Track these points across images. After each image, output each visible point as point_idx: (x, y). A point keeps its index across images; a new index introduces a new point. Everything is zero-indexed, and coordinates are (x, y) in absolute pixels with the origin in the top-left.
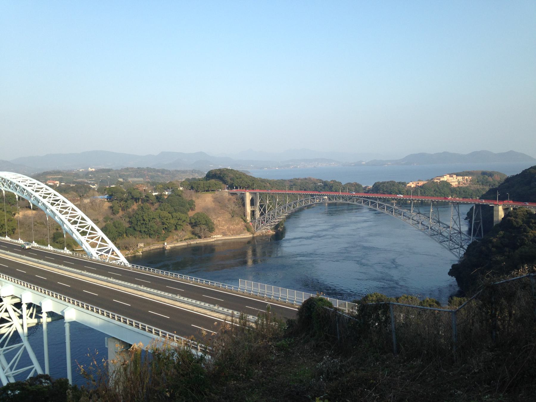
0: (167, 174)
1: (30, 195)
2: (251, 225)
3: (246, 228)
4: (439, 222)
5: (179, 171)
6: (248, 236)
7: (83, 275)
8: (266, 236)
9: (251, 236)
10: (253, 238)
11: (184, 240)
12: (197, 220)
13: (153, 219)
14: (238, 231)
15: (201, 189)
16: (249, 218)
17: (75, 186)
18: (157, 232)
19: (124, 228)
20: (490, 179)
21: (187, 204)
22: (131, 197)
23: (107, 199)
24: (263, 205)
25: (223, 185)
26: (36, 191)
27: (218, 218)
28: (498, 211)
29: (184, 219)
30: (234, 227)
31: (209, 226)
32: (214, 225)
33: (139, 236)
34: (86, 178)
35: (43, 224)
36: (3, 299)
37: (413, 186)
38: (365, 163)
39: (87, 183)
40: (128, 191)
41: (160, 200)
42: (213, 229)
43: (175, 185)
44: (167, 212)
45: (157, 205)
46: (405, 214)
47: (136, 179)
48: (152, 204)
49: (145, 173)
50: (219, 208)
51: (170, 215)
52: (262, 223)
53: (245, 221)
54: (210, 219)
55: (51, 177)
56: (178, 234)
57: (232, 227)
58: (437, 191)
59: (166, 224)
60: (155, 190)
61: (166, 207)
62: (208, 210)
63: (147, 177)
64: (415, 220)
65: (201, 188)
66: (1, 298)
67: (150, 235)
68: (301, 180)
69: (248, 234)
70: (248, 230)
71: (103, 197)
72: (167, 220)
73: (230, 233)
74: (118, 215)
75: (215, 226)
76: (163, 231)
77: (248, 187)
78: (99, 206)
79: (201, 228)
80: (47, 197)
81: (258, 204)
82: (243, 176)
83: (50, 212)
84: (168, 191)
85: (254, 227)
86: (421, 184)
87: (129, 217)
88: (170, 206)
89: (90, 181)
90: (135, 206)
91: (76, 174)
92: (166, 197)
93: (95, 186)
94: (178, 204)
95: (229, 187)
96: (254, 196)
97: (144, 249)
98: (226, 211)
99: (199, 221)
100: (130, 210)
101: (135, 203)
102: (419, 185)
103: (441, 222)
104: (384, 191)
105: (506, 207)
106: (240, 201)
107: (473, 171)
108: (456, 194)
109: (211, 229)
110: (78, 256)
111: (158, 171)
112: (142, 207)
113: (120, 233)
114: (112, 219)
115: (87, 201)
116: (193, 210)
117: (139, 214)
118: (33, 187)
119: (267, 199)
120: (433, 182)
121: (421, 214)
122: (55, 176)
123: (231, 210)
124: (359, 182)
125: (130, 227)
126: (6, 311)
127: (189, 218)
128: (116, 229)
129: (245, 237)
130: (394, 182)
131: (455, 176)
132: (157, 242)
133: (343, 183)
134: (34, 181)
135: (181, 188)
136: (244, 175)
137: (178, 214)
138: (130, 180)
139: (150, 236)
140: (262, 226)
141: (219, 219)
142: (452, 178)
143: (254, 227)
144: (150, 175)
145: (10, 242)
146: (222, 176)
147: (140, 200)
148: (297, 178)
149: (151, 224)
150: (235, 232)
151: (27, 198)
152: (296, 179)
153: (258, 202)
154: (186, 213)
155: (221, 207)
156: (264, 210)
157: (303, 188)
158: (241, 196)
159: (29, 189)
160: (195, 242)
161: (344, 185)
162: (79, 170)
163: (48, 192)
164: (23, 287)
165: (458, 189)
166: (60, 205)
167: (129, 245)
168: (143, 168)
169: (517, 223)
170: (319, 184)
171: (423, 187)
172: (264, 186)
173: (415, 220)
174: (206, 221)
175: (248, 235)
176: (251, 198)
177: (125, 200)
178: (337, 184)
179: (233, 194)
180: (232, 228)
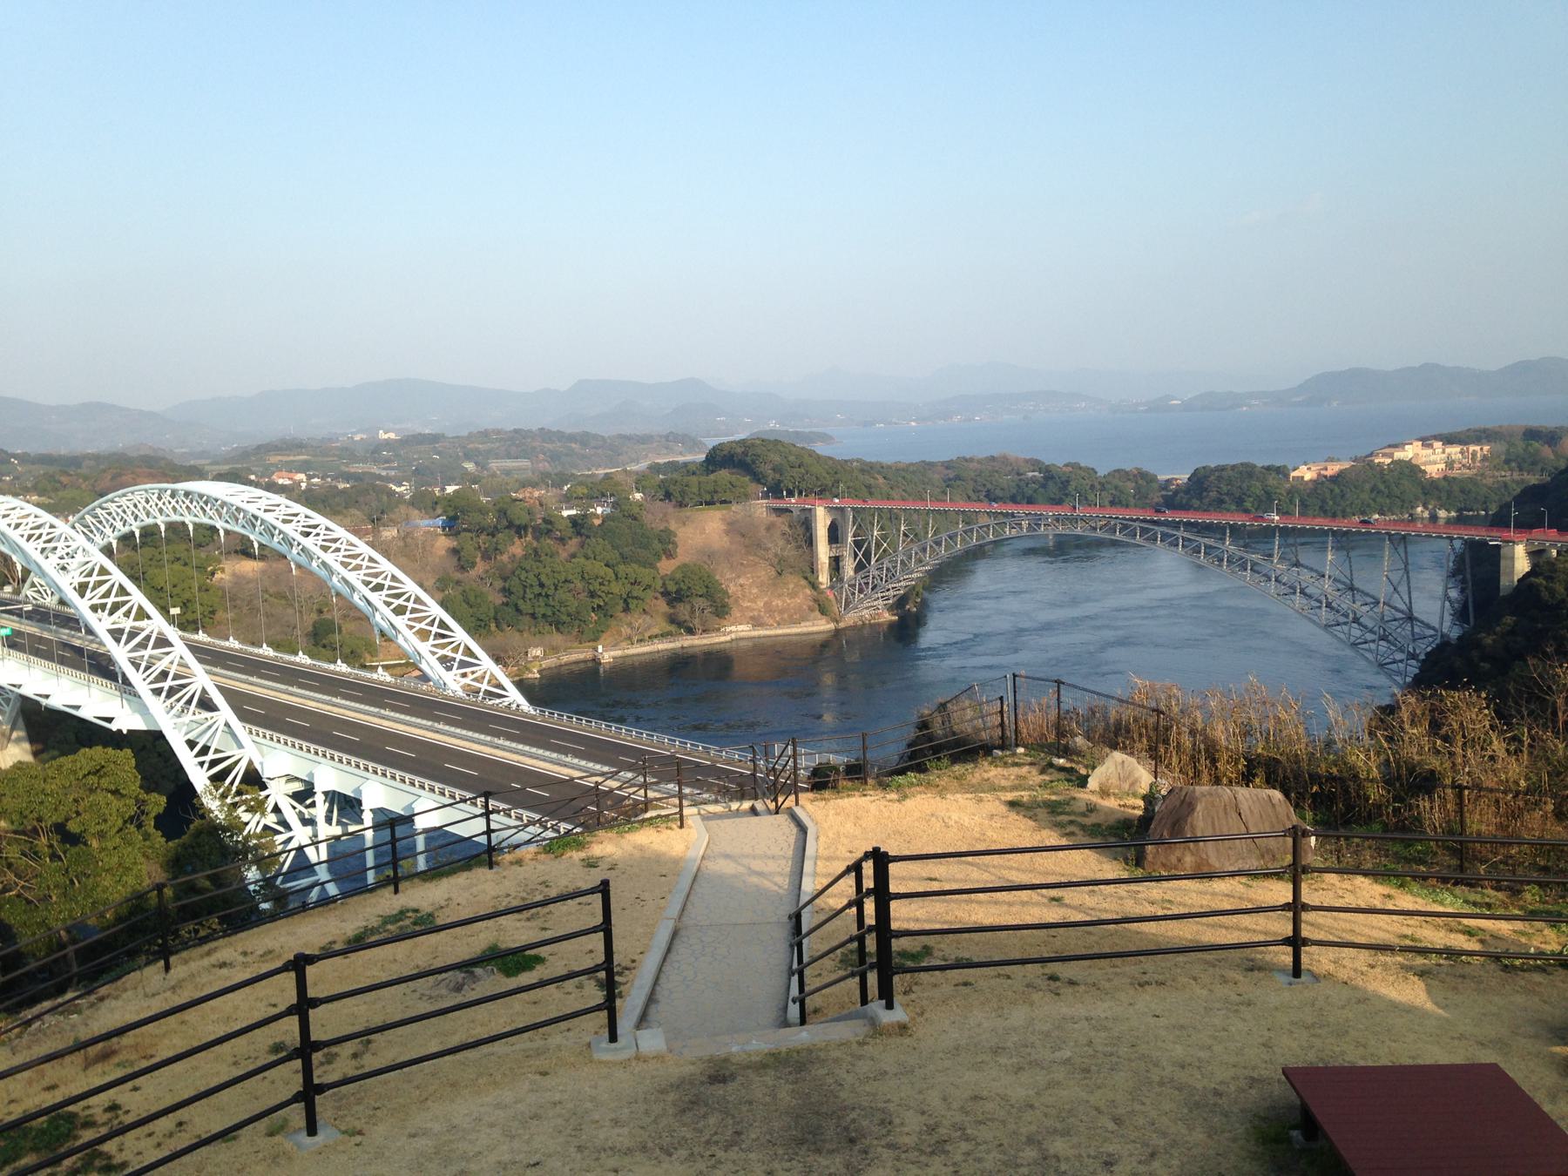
0: (595, 448)
1: (289, 542)
2: (831, 597)
4: (1352, 588)
5: (628, 438)
7: (438, 732)
9: (832, 626)
10: (837, 633)
12: (682, 585)
16: (824, 578)
17: (352, 487)
18: (576, 617)
19: (492, 606)
20: (1547, 452)
21: (656, 542)
23: (444, 529)
24: (864, 541)
26: (285, 521)
27: (739, 577)
28: (1512, 558)
29: (647, 580)
30: (784, 601)
32: (729, 597)
33: (530, 628)
34: (375, 461)
35: (285, 597)
37: (1308, 476)
39: (380, 477)
40: (497, 507)
43: (622, 485)
45: (573, 544)
46: (1256, 568)
47: (510, 464)
48: (562, 540)
49: (534, 444)
50: (743, 552)
52: (861, 591)
53: (814, 585)
55: (280, 458)
56: (631, 623)
57: (778, 603)
59: (600, 597)
60: (568, 500)
61: (599, 549)
62: (711, 555)
63: (541, 456)
64: (1284, 584)
65: (692, 496)
66: (264, 780)
67: (558, 625)
68: (979, 462)
69: (823, 622)
71: (431, 522)
72: (601, 584)
74: (473, 573)
75: (732, 599)
76: (593, 615)
77: (823, 492)
78: (424, 548)
79: (693, 607)
80: (330, 547)
82: (807, 460)
83: (339, 584)
85: (838, 601)
86: (1333, 469)
88: (609, 547)
89: (384, 469)
90: (517, 548)
91: (347, 449)
92: (597, 522)
93: (403, 488)
94: (630, 541)
95: (768, 491)
96: (839, 518)
97: (545, 664)
98: (761, 558)
99: (689, 588)
100: (505, 558)
101: (516, 539)
102: (1329, 473)
103: (1358, 590)
105: (1536, 545)
106: (800, 530)
107: (1500, 427)
108: (1439, 498)
109: (721, 610)
110: (409, 684)
111: (572, 438)
112: (535, 551)
114: (458, 583)
115: (389, 533)
120: (1371, 465)
121: (1302, 566)
122: (289, 455)
123: (776, 555)
126: (276, 810)
127: (662, 578)
128: (471, 610)
129: (815, 629)
131: (1438, 445)
132: (576, 644)
133: (1102, 472)
135: (638, 496)
136: (810, 456)
137: (633, 570)
138: (494, 465)
139: (558, 629)
140: (861, 601)
141: (741, 581)
142: (1432, 451)
143: (838, 601)
144: (549, 450)
145: (209, 644)
146: (748, 459)
147: (530, 530)
148: (968, 457)
149: (561, 594)
150: (786, 616)
152: (966, 460)
153: (850, 535)
154: (652, 566)
155: (746, 547)
156: (867, 555)
158: (803, 517)
159: (269, 517)
162: (352, 438)
164: (315, 758)
165: (1444, 484)
166: (342, 550)
167: (506, 652)
169: (1552, 592)
170: (1030, 474)
171: (1340, 479)
172: (869, 487)
174: (707, 587)
175: (820, 626)
177: (490, 530)
178: (1083, 474)
179: (779, 511)
180: (777, 606)
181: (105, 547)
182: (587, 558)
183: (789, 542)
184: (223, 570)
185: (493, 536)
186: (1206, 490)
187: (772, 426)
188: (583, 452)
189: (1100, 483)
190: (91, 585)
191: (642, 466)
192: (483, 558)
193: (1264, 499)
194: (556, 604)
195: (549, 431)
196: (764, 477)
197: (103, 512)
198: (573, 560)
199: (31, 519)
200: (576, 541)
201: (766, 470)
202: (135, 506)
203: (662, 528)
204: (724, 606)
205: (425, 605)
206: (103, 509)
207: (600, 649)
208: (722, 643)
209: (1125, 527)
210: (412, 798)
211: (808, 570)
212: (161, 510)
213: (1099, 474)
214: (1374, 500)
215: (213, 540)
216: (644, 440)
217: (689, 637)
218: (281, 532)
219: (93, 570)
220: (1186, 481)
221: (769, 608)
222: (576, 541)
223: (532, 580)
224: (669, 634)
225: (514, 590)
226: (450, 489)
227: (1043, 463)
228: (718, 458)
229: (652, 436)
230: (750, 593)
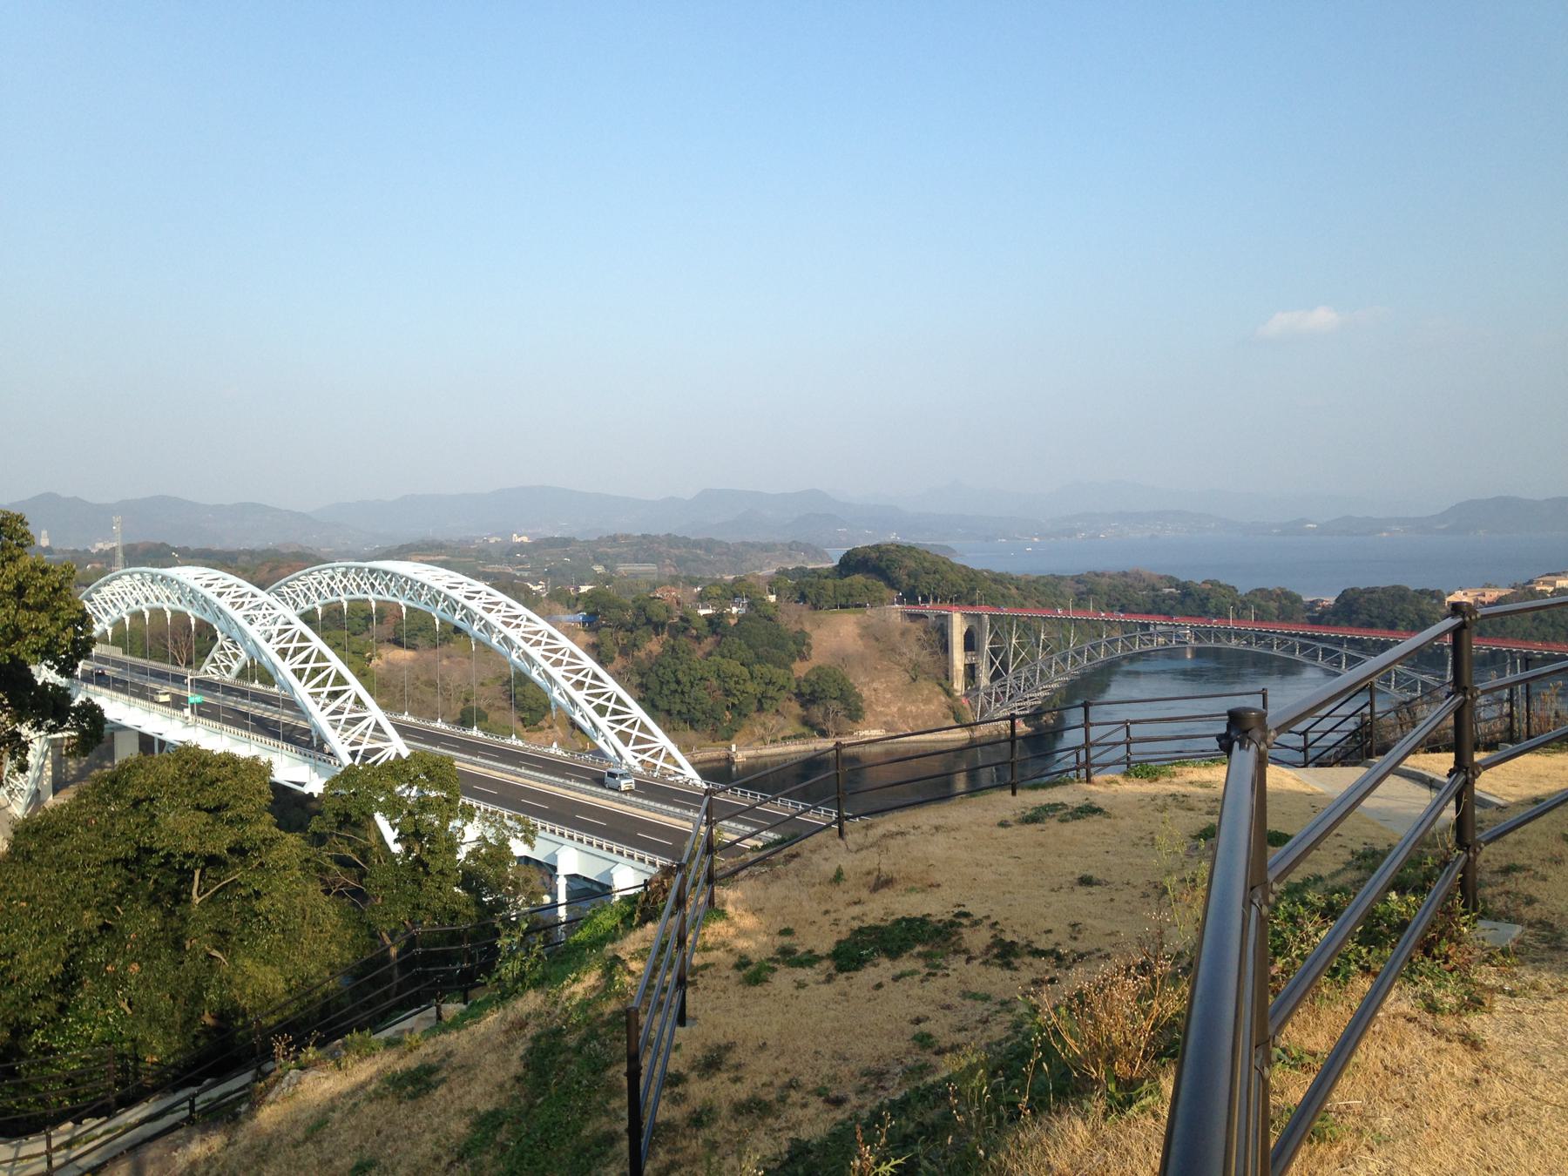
1: (470, 616)
2: (966, 705)
3: (951, 714)
5: (753, 546)
6: (957, 736)
11: (783, 738)
15: (826, 602)
16: (959, 685)
21: (791, 643)
23: (584, 624)
24: (1001, 649)
25: (887, 593)
27: (873, 681)
29: (781, 681)
30: (918, 707)
34: (510, 563)
40: (637, 604)
41: (719, 630)
45: (708, 643)
48: (698, 639)
51: (745, 670)
52: (997, 701)
53: (949, 693)
54: (851, 684)
58: (1542, 620)
59: (735, 695)
60: (702, 599)
61: (734, 648)
62: (845, 659)
63: (668, 561)
67: (692, 723)
68: (1110, 577)
71: (571, 617)
72: (737, 683)
76: (727, 713)
79: (827, 709)
83: (518, 661)
85: (973, 709)
87: (639, 674)
89: (519, 570)
90: (654, 646)
92: (733, 622)
93: (539, 587)
95: (903, 597)
96: (975, 624)
98: (895, 664)
99: (824, 690)
100: (642, 654)
104: (1371, 617)
106: (936, 636)
109: (855, 714)
111: (697, 544)
127: (796, 679)
130: (1406, 590)
135: (773, 598)
136: (944, 563)
137: (768, 670)
138: (623, 568)
139: (692, 727)
141: (875, 685)
143: (973, 709)
146: (883, 564)
148: (1099, 571)
149: (698, 692)
152: (1097, 575)
153: (987, 642)
154: (787, 667)
155: (881, 651)
156: (1004, 664)
158: (939, 623)
161: (1246, 595)
168: (657, 537)
170: (1167, 590)
172: (1003, 596)
175: (960, 735)
180: (911, 711)
181: (308, 612)
182: (723, 657)
183: (923, 647)
184: (380, 657)
185: (632, 632)
186: (1355, 612)
187: (893, 537)
188: (707, 558)
189: (1241, 601)
190: (290, 652)
191: (770, 571)
192: (620, 653)
193: (1418, 624)
194: (692, 701)
195: (676, 537)
196: (898, 583)
197: (289, 590)
198: (710, 658)
199: (234, 589)
200: (710, 640)
201: (902, 575)
202: (320, 583)
203: (798, 629)
204: (859, 709)
205: (602, 681)
206: (289, 587)
207: (734, 748)
209: (1283, 642)
210: (609, 865)
211: (943, 676)
212: (345, 588)
213: (1239, 593)
214: (1537, 629)
215: (368, 630)
216: (766, 548)
218: (463, 607)
219: (294, 636)
220: (1332, 603)
222: (710, 640)
223: (669, 676)
224: (802, 736)
225: (650, 686)
226: (584, 589)
227: (1178, 580)
228: (852, 563)
229: (775, 545)
230: (885, 698)
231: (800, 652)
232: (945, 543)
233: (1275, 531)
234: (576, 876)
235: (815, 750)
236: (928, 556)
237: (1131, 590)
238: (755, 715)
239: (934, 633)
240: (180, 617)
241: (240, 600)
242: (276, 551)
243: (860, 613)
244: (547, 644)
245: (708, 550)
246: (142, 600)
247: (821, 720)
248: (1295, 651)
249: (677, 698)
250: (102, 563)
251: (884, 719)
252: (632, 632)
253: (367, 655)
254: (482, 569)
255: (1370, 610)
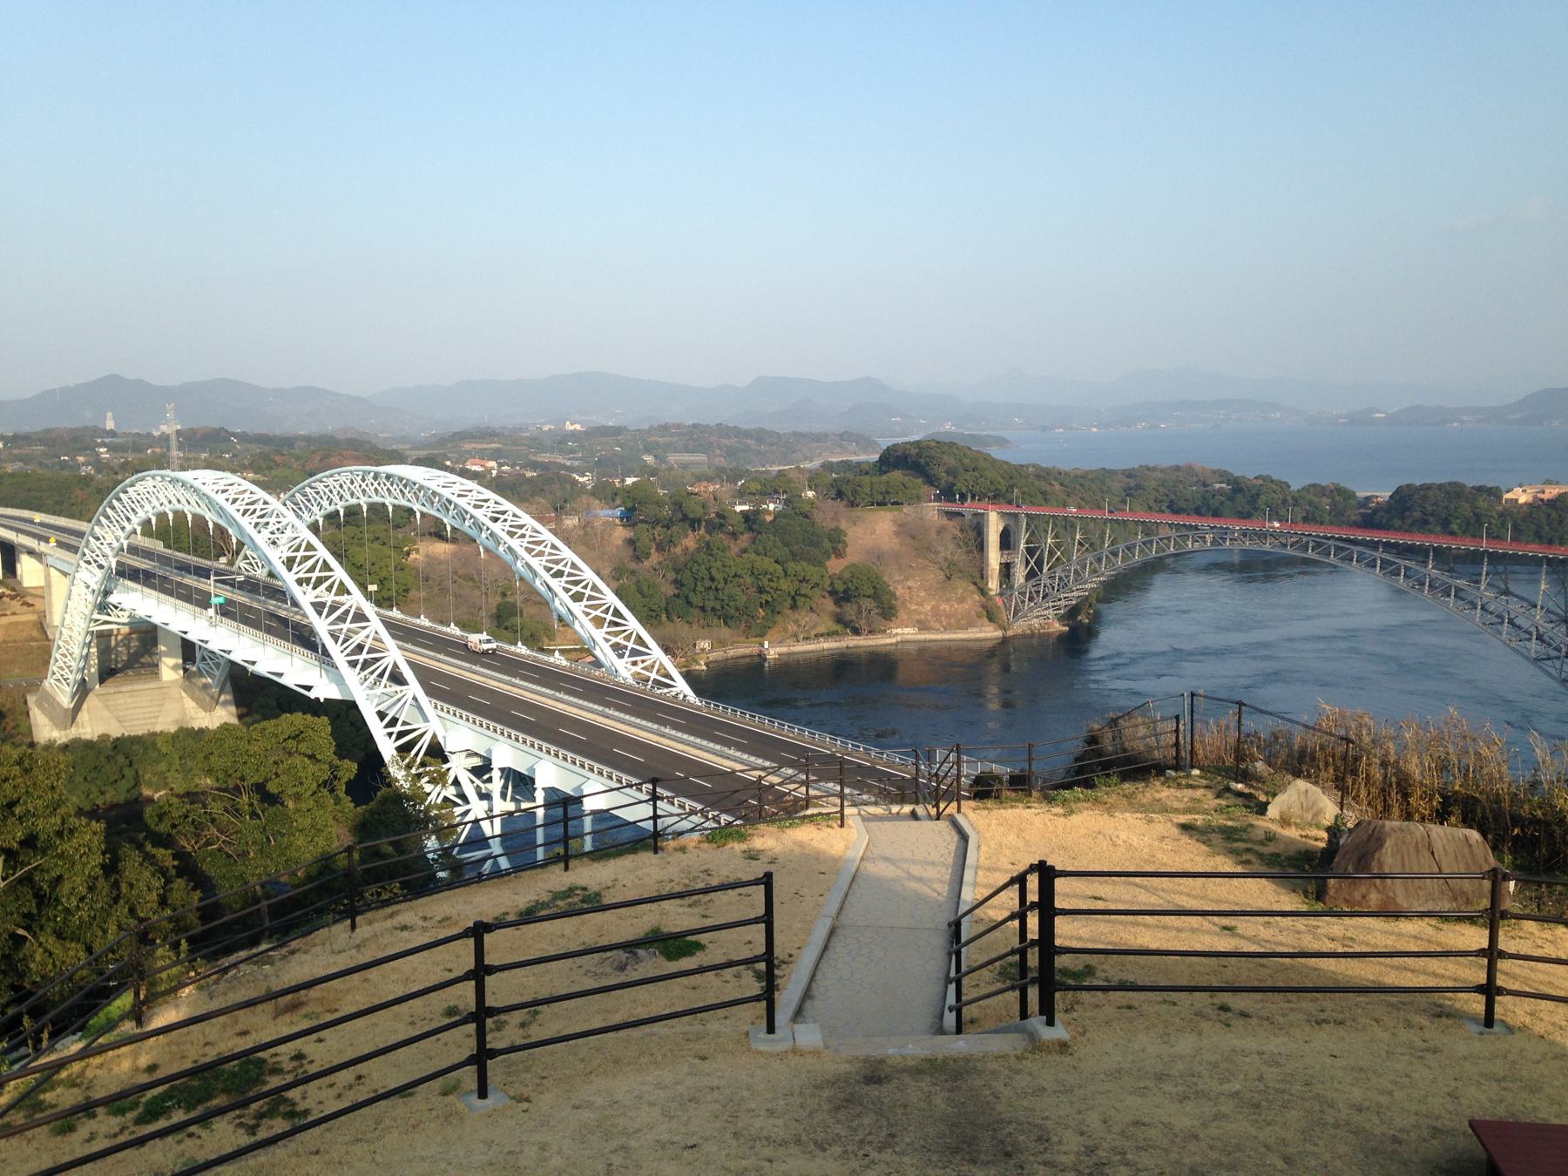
0: (771, 445)
1: (479, 527)
2: (1000, 604)
3: (985, 613)
5: (803, 436)
6: (989, 635)
8: (1041, 636)
9: (999, 633)
10: (1005, 641)
11: (816, 636)
13: (735, 576)
14: (963, 619)
15: (863, 499)
16: (993, 585)
17: (538, 476)
21: (827, 540)
22: (680, 516)
24: (1037, 548)
25: (926, 490)
26: (476, 507)
27: (907, 579)
29: (815, 579)
31: (882, 603)
34: (561, 452)
35: (472, 579)
36: (451, 757)
37: (1523, 499)
38: (1383, 415)
39: (564, 467)
40: (673, 500)
41: (754, 526)
42: (893, 611)
44: (772, 560)
47: (687, 458)
48: (734, 535)
51: (779, 568)
52: (1031, 599)
53: (983, 591)
54: (884, 582)
55: (473, 445)
57: (945, 607)
59: (768, 592)
60: (741, 495)
62: (880, 556)
63: (718, 451)
64: (1491, 613)
67: (727, 620)
68: (1162, 471)
69: (991, 628)
70: (991, 617)
72: (770, 580)
73: (941, 622)
74: (647, 563)
76: (761, 610)
78: (602, 538)
79: (860, 607)
81: (1022, 546)
84: (775, 503)
85: (1008, 609)
86: (1551, 492)
87: (675, 570)
88: (779, 544)
89: (569, 459)
90: (690, 541)
92: (769, 518)
93: (586, 478)
96: (1012, 523)
97: (712, 656)
98: (930, 561)
99: (857, 588)
100: (678, 550)
102: (1546, 496)
104: (1425, 514)
106: (972, 534)
109: (887, 611)
110: (582, 669)
111: (747, 434)
112: (708, 544)
113: (654, 611)
114: (633, 572)
115: (571, 522)
116: (840, 555)
117: (700, 561)
118: (469, 497)
119: (1047, 532)
122: (482, 443)
124: (1349, 485)
125: (677, 596)
127: (830, 577)
130: (1463, 486)
134: (488, 494)
135: (810, 494)
137: (802, 567)
138: (673, 458)
139: (726, 623)
140: (1031, 610)
141: (909, 583)
143: (1008, 609)
145: (401, 621)
146: (922, 461)
147: (704, 524)
148: (1151, 465)
149: (732, 589)
150: (952, 621)
151: (473, 533)
152: (1148, 469)
153: (1023, 541)
154: (821, 564)
155: (917, 549)
156: (1039, 563)
157: (1164, 498)
158: (975, 521)
159: (462, 502)
160: (843, 644)
161: (1298, 491)
162: (541, 428)
163: (501, 508)
164: (494, 735)
167: (675, 643)
168: (707, 426)
170: (1217, 486)
171: (1558, 504)
172: (1044, 493)
173: (1491, 613)
174: (874, 588)
175: (988, 633)
176: (1001, 528)
178: (1275, 487)
180: (945, 610)
183: (959, 546)
184: (417, 551)
186: (1409, 509)
187: (947, 428)
194: (726, 598)
197: (312, 491)
198: (744, 555)
199: (247, 495)
201: (940, 472)
203: (833, 527)
204: (892, 607)
206: (312, 488)
207: (766, 644)
208: (887, 645)
209: (1318, 545)
211: (978, 575)
212: (364, 491)
215: (410, 522)
216: (819, 438)
217: (855, 638)
220: (1387, 499)
221: (936, 613)
223: (703, 572)
224: (835, 633)
226: (629, 481)
227: (1232, 475)
229: (826, 435)
231: (834, 549)
232: (1000, 434)
233: (1342, 420)
234: (553, 789)
235: (848, 647)
236: (969, 452)
237: (1181, 486)
238: (788, 612)
239: (970, 533)
240: (200, 521)
241: (252, 507)
242: (332, 437)
243: (895, 510)
244: (550, 554)
245: (760, 441)
246: (166, 502)
247: (854, 618)
248: (1330, 554)
249: (711, 595)
250: (161, 448)
251: (918, 617)
252: (668, 528)
253: (405, 549)
254: (534, 458)
255: (1423, 507)
